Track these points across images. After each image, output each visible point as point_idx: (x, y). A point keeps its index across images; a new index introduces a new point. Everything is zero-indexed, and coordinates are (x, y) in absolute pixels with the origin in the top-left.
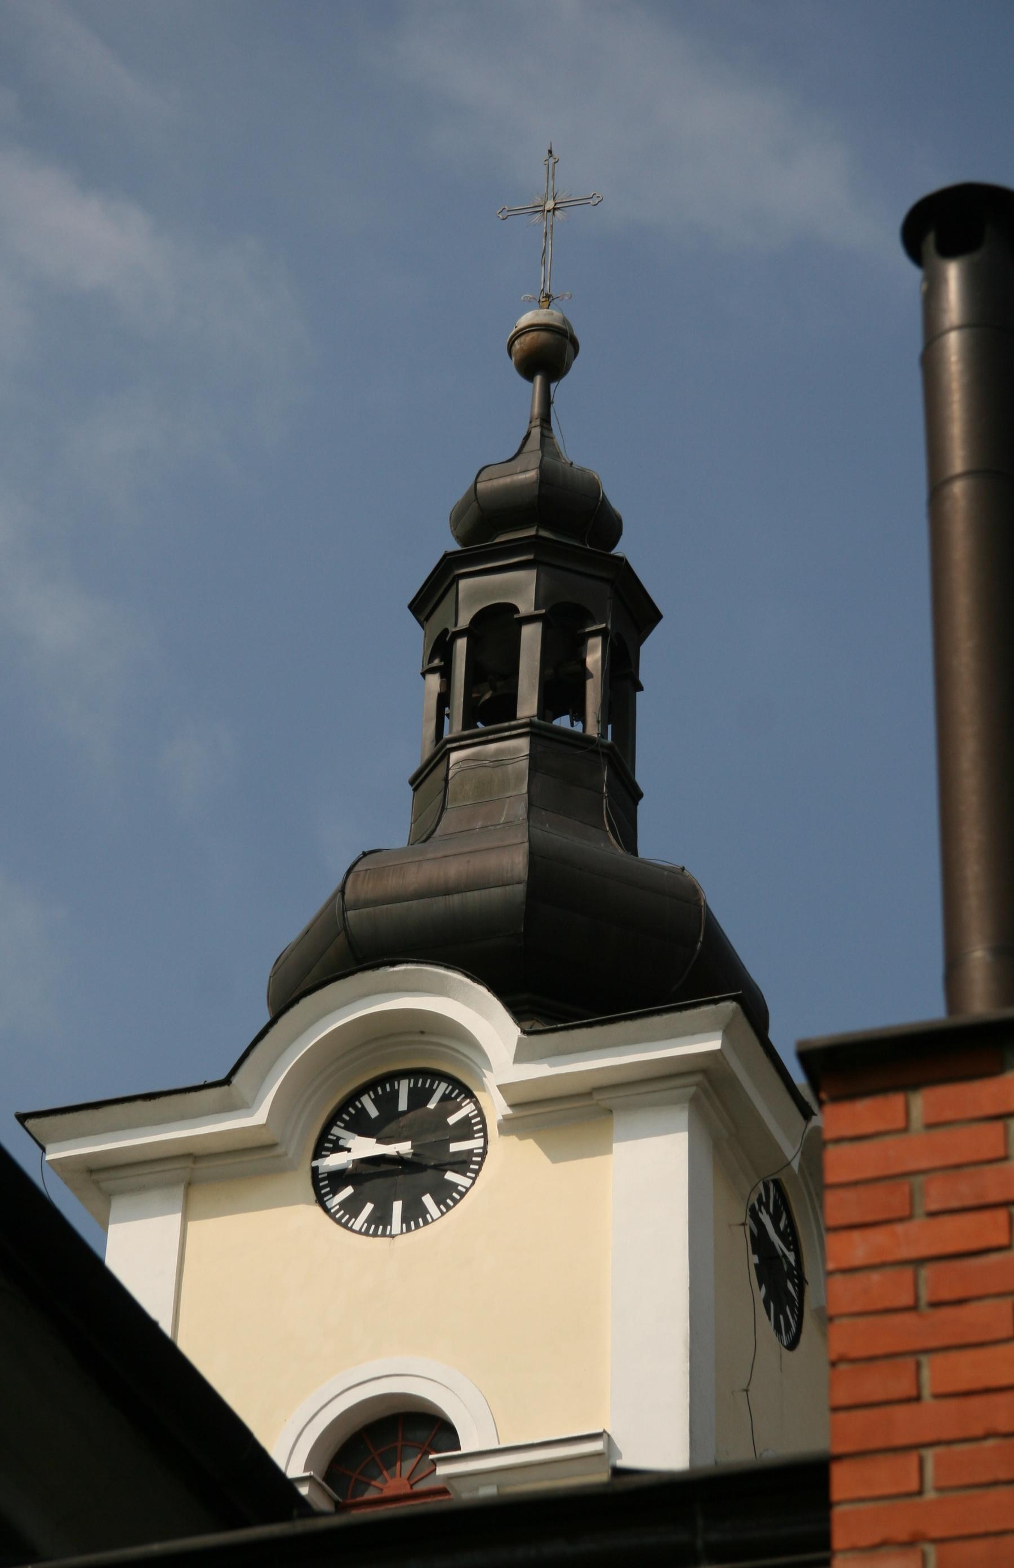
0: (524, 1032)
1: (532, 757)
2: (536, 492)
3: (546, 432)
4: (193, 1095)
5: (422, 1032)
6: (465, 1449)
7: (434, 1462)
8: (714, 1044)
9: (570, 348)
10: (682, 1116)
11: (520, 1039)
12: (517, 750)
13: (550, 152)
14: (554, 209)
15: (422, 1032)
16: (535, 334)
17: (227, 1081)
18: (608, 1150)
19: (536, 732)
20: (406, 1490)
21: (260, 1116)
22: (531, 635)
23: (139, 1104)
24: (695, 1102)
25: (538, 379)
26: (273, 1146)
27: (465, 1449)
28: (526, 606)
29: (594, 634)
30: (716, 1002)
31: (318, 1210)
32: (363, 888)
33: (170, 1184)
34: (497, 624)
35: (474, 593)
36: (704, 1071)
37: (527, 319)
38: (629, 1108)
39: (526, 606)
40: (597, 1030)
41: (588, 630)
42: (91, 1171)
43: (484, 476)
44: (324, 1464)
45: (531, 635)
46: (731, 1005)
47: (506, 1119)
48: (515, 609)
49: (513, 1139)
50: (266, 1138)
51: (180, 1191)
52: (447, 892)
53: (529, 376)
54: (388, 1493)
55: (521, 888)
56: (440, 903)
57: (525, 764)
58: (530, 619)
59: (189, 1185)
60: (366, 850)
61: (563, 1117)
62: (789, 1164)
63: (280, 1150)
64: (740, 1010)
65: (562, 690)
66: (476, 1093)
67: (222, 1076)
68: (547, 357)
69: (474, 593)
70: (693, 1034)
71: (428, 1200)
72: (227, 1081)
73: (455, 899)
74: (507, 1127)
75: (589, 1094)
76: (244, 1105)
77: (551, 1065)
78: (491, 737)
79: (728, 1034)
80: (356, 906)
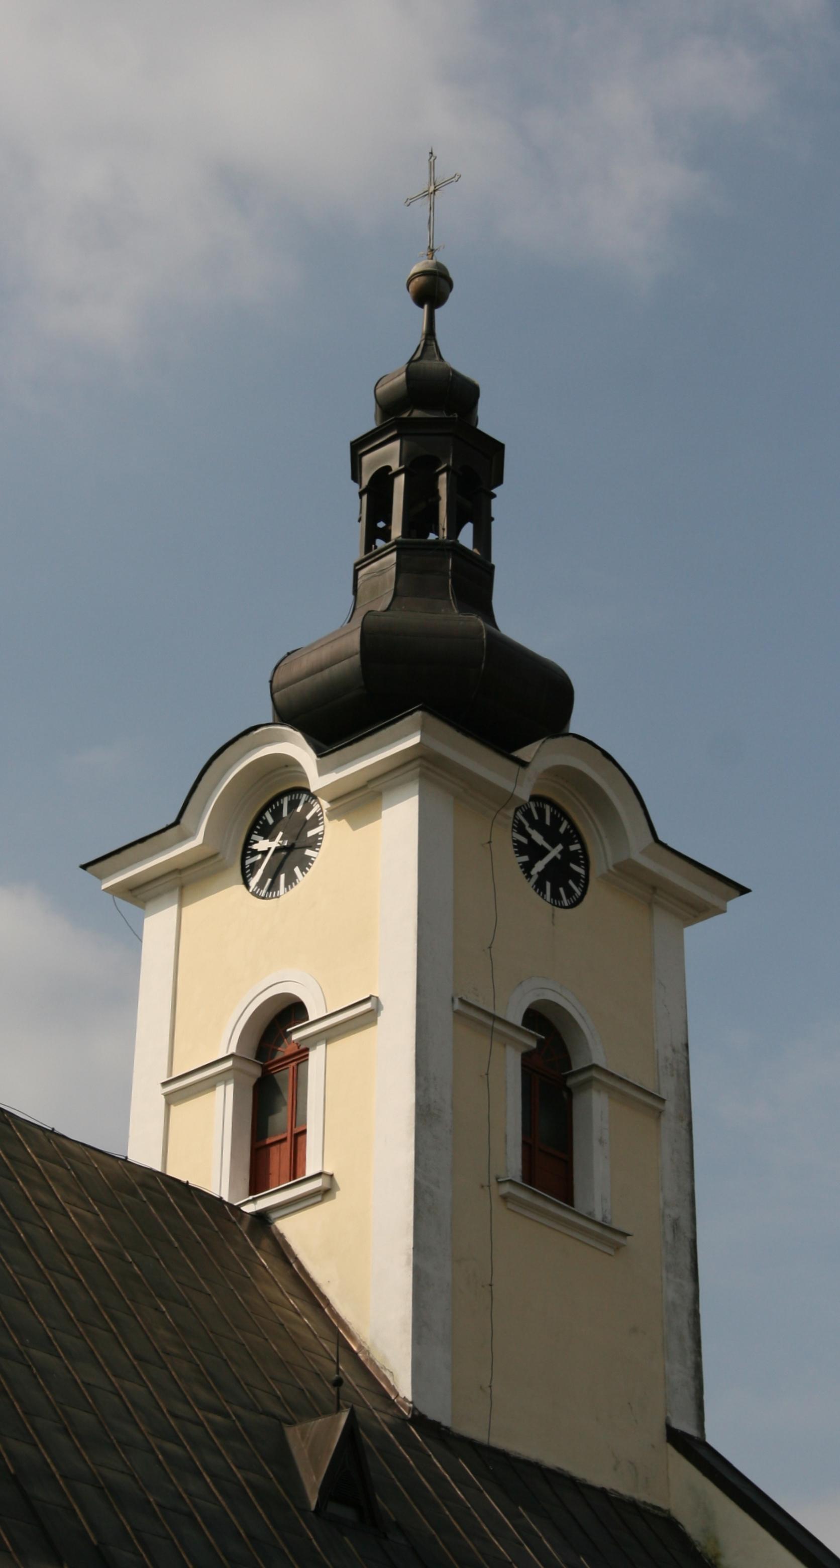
0: (318, 756)
1: (398, 564)
2: (406, 387)
3: (429, 342)
4: (163, 835)
5: (287, 766)
6: (311, 1019)
7: (291, 1032)
8: (415, 740)
9: (443, 282)
10: (415, 787)
11: (317, 762)
12: (391, 561)
13: (431, 153)
14: (435, 191)
15: (287, 766)
16: (417, 280)
17: (177, 822)
18: (379, 817)
19: (400, 547)
20: (297, 1050)
21: (199, 840)
22: (400, 482)
23: (139, 846)
24: (423, 776)
25: (426, 306)
26: (215, 855)
27: (311, 1019)
28: (395, 466)
29: (442, 472)
30: (411, 713)
31: (243, 887)
32: (281, 678)
33: (170, 890)
34: (383, 478)
35: (371, 462)
36: (421, 757)
37: (415, 269)
38: (391, 788)
39: (395, 466)
40: (355, 746)
41: (438, 470)
42: (131, 890)
43: (379, 385)
44: (254, 1043)
45: (400, 482)
46: (419, 714)
47: (329, 810)
48: (388, 468)
49: (336, 821)
50: (209, 851)
51: (176, 893)
52: (321, 669)
53: (422, 306)
54: (287, 1053)
55: (358, 657)
56: (319, 677)
57: (394, 569)
58: (398, 473)
59: (182, 887)
60: (290, 651)
61: (360, 801)
62: (512, 794)
63: (220, 857)
64: (426, 714)
65: (420, 517)
66: (319, 798)
67: (173, 819)
68: (432, 289)
69: (371, 462)
70: (406, 736)
71: (297, 870)
72: (177, 822)
73: (326, 673)
74: (334, 814)
75: (364, 787)
76: (186, 837)
77: (334, 774)
78: (385, 552)
79: (424, 730)
80: (279, 689)
